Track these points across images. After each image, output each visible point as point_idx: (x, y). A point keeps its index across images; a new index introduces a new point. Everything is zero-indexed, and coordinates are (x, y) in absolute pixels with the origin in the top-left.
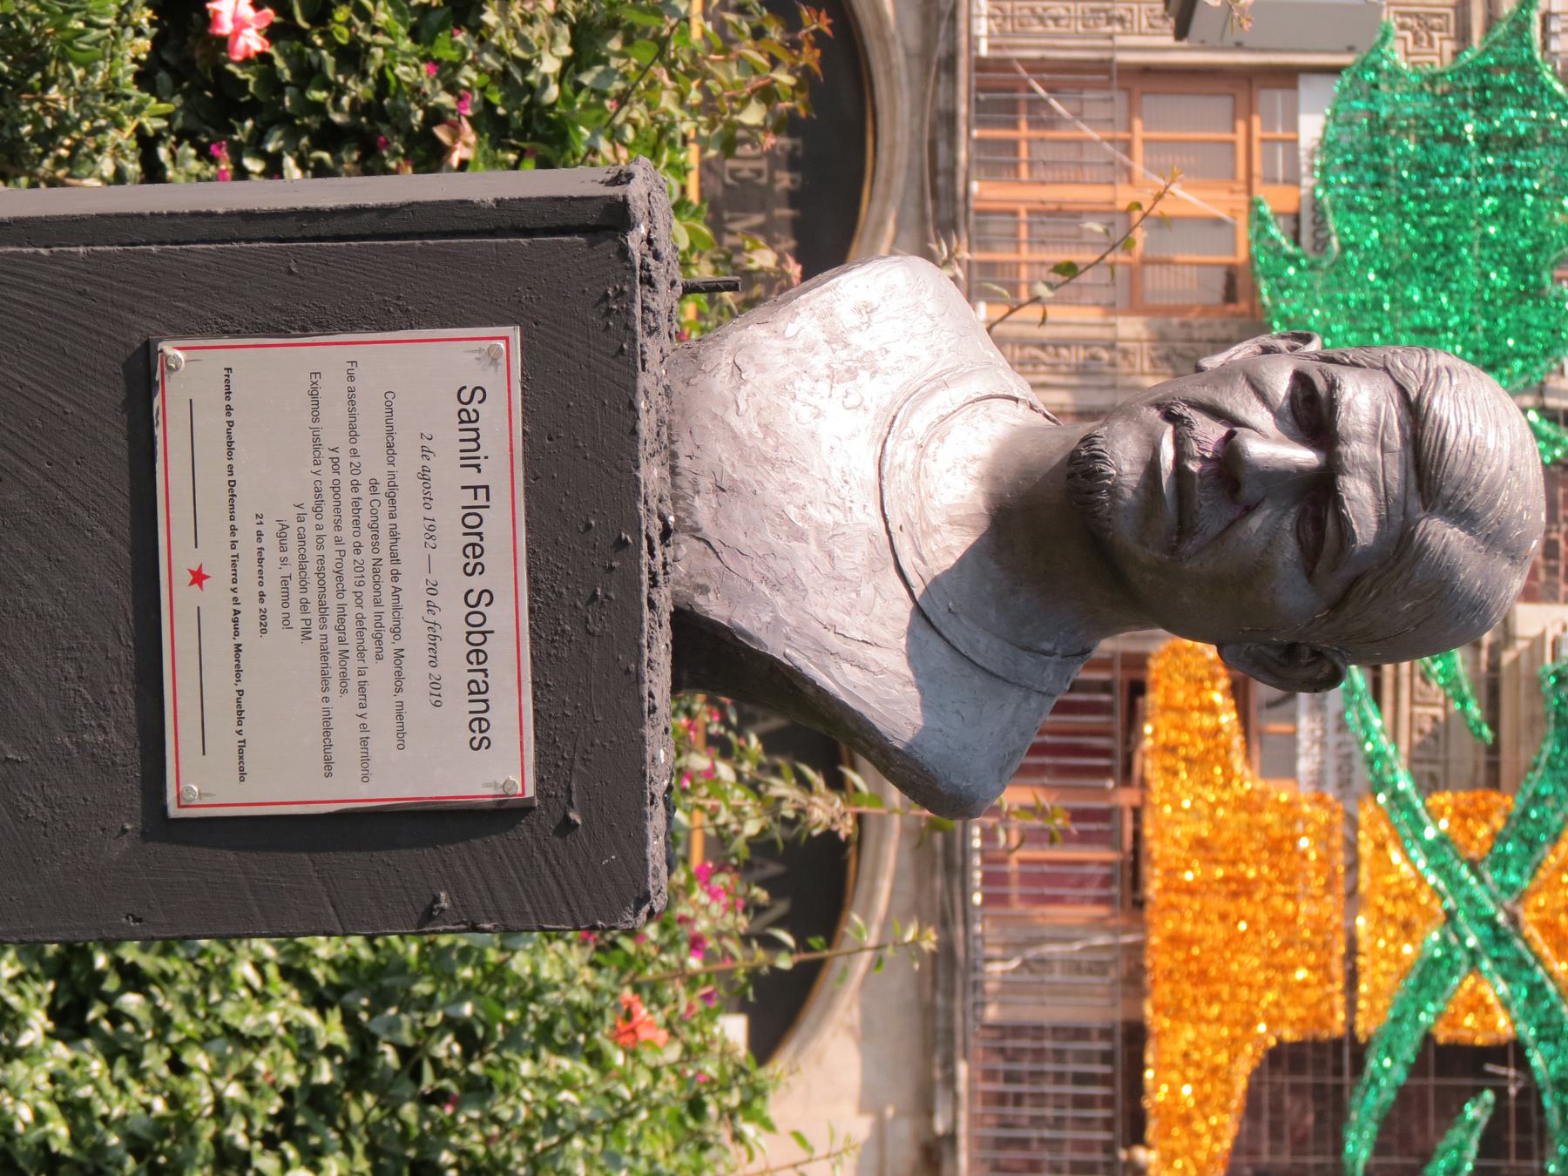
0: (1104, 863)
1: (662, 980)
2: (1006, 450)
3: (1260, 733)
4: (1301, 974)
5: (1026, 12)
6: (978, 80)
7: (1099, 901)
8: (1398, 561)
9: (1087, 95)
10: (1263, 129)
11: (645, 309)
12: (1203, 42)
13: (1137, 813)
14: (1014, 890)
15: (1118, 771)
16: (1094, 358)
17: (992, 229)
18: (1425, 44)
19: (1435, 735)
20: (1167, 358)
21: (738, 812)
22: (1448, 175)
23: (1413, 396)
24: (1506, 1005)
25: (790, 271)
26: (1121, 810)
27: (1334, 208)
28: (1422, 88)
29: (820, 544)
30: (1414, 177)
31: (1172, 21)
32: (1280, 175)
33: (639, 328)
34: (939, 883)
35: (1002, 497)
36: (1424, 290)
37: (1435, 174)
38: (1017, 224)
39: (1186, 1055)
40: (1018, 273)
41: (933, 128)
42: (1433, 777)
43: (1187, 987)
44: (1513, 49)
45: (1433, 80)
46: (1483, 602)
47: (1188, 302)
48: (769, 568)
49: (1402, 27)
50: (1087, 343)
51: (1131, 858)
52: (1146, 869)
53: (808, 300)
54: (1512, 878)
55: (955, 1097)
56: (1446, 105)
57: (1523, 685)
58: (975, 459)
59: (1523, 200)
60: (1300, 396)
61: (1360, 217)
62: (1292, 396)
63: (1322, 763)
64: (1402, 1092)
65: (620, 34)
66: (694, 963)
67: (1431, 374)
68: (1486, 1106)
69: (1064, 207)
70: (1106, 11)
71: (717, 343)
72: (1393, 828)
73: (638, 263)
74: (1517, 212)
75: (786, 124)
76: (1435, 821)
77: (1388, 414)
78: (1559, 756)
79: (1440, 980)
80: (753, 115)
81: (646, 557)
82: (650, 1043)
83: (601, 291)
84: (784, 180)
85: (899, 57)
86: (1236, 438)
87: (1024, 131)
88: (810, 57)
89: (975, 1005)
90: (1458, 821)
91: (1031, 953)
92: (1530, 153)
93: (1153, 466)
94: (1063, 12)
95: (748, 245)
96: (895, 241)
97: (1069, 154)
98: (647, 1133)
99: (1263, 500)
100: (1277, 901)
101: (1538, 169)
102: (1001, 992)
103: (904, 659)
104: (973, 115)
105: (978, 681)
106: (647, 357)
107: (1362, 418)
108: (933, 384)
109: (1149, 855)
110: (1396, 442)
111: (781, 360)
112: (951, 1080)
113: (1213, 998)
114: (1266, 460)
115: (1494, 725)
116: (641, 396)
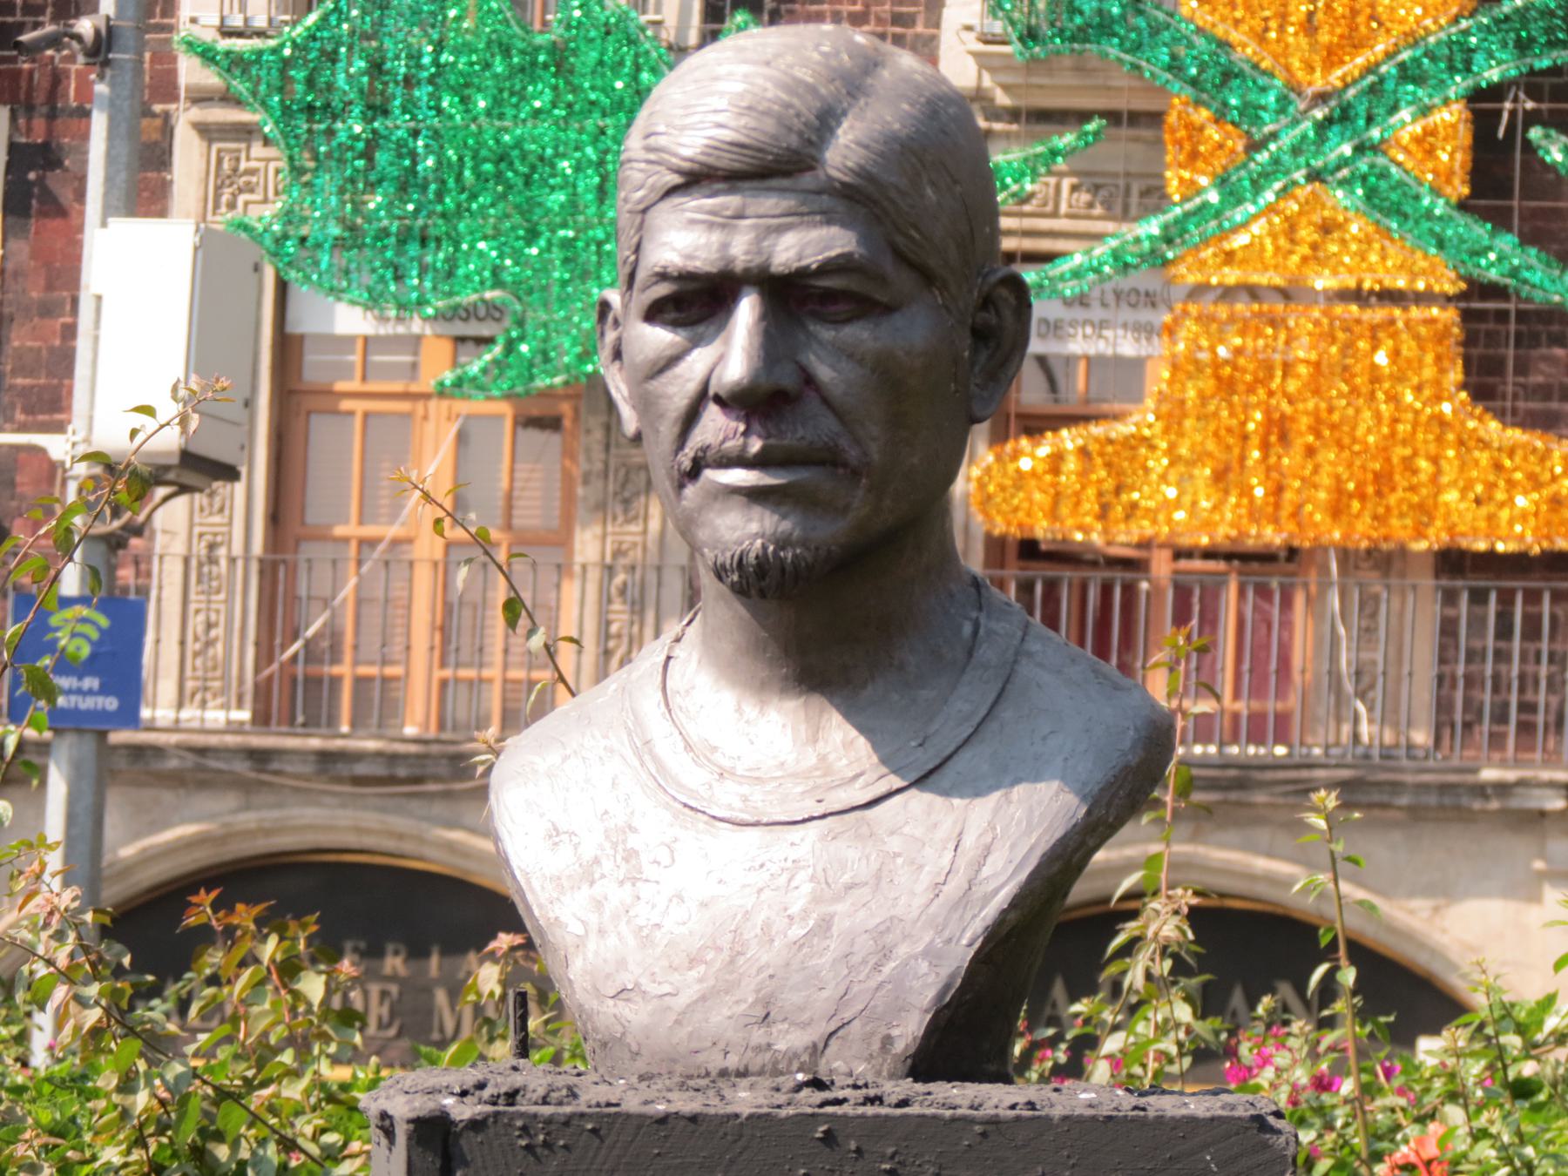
0: (1242, 593)
1: (1365, 1124)
2: (729, 671)
3: (1087, 401)
4: (1381, 358)
5: (199, 662)
6: (279, 723)
7: (1287, 603)
8: (875, 202)
9: (302, 591)
10: (350, 378)
11: (545, 1101)
12: (242, 448)
13: (1179, 554)
14: (1271, 706)
15: (1129, 575)
16: (623, 591)
17: (462, 715)
18: (254, 179)
19: (1096, 189)
20: (627, 502)
21: (1163, 1029)
22: (413, 155)
23: (676, 179)
24: (1425, 111)
25: (505, 947)
26: (1176, 572)
27: (450, 294)
28: (307, 184)
29: (838, 899)
30: (416, 196)
31: (216, 485)
32: (408, 359)
33: (568, 1109)
34: (1260, 797)
35: (786, 678)
36: (553, 189)
37: (412, 170)
38: (457, 680)
39: (1478, 501)
40: (516, 682)
41: (338, 780)
42: (1145, 193)
43: (1392, 499)
44: (263, 73)
45: (297, 171)
46: (929, 102)
47: (558, 476)
48: (864, 962)
49: (232, 206)
50: (605, 600)
51: (1236, 563)
52: (1251, 543)
53: (541, 906)
54: (1271, 99)
55: (1522, 783)
56: (329, 155)
57: (1035, 80)
58: (739, 710)
59: (446, 65)
60: (673, 315)
61: (461, 262)
62: (675, 324)
63: (1125, 326)
64: (1526, 240)
65: (211, 1146)
66: (1347, 1087)
67: (652, 157)
68: (1547, 136)
69: (438, 622)
70: (200, 565)
71: (590, 1017)
72: (1206, 242)
73: (489, 1109)
74: (461, 73)
75: (326, 951)
76: (1199, 191)
77: (699, 210)
78: (1122, 40)
79: (1393, 188)
80: (313, 986)
81: (845, 1109)
82: (1443, 1142)
83: (523, 1153)
84: (394, 963)
85: (248, 819)
86: (722, 393)
87: (344, 670)
88: (244, 916)
89: (1410, 757)
90: (1200, 164)
91: (1349, 687)
92: (390, 55)
93: (755, 495)
94: (201, 618)
95: (472, 997)
96: (472, 830)
97: (373, 615)
98: (1551, 1149)
99: (797, 363)
100: (1292, 386)
101: (409, 46)
102: (1396, 725)
103: (978, 801)
104: (324, 731)
105: (1007, 713)
106: (603, 1100)
107: (703, 240)
108: (647, 758)
109: (1233, 540)
110: (732, 201)
111: (612, 940)
112: (1502, 788)
113: (1409, 466)
114: (750, 358)
115: (1084, 116)
116: (649, 1110)
